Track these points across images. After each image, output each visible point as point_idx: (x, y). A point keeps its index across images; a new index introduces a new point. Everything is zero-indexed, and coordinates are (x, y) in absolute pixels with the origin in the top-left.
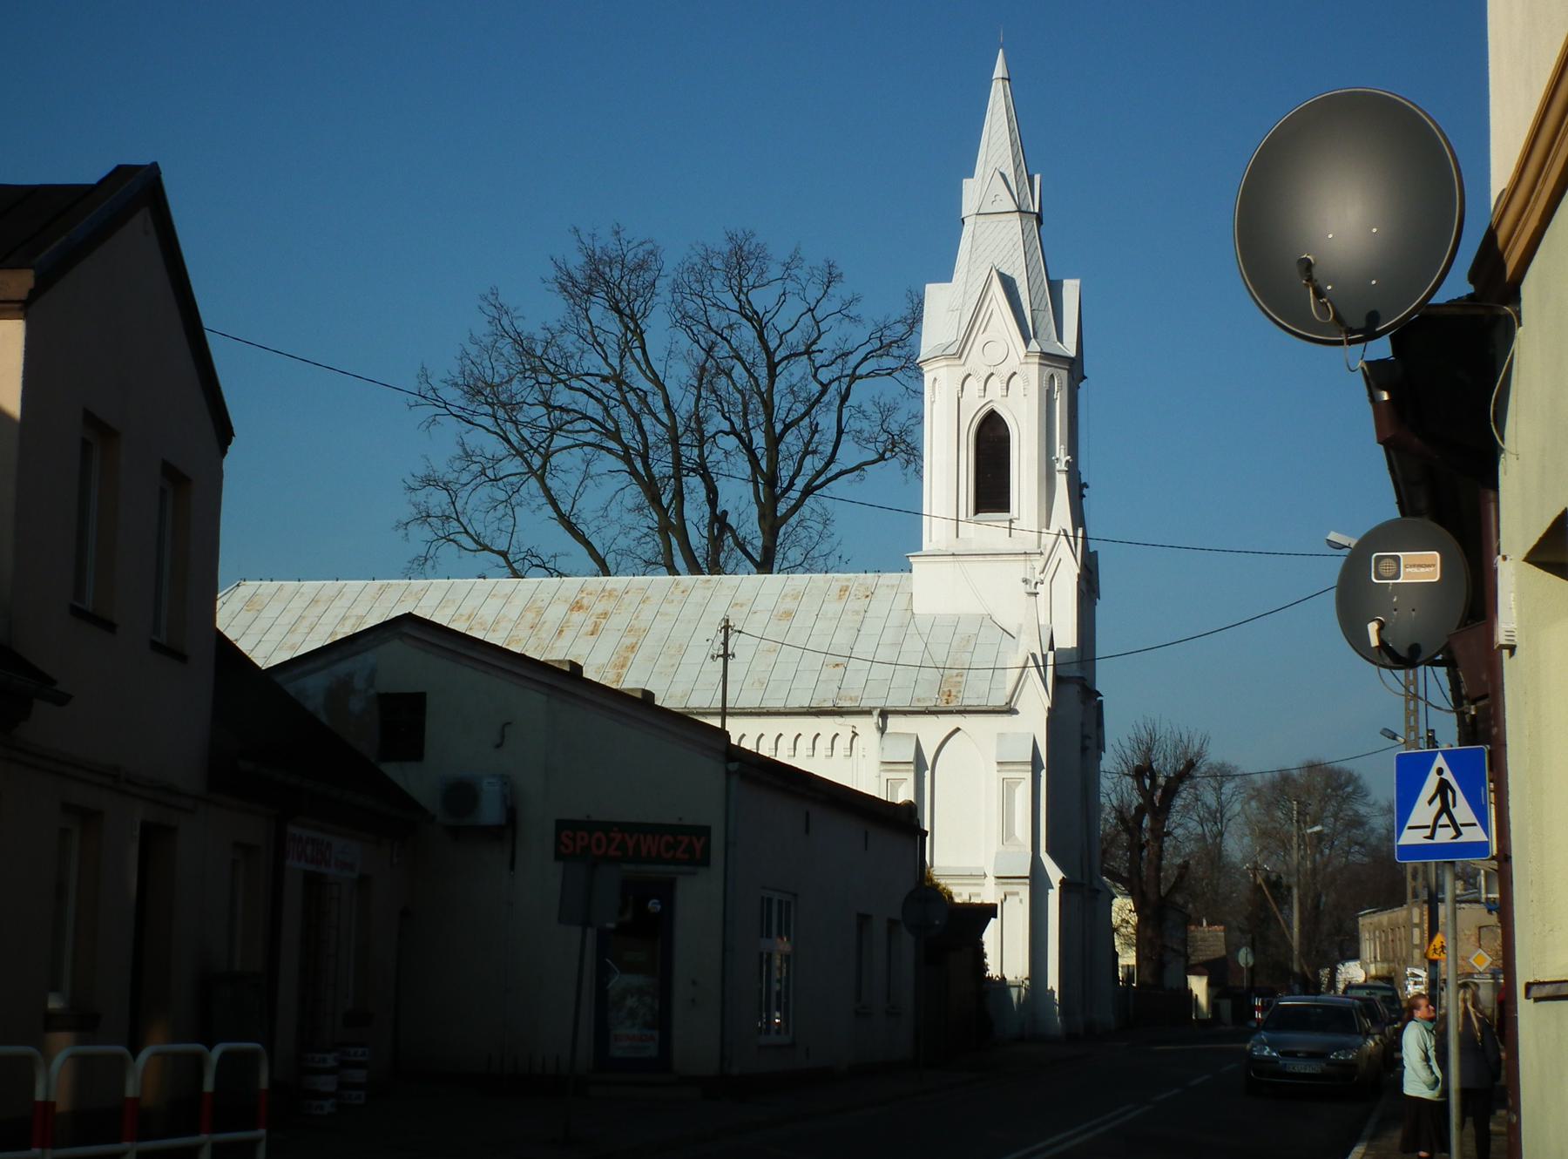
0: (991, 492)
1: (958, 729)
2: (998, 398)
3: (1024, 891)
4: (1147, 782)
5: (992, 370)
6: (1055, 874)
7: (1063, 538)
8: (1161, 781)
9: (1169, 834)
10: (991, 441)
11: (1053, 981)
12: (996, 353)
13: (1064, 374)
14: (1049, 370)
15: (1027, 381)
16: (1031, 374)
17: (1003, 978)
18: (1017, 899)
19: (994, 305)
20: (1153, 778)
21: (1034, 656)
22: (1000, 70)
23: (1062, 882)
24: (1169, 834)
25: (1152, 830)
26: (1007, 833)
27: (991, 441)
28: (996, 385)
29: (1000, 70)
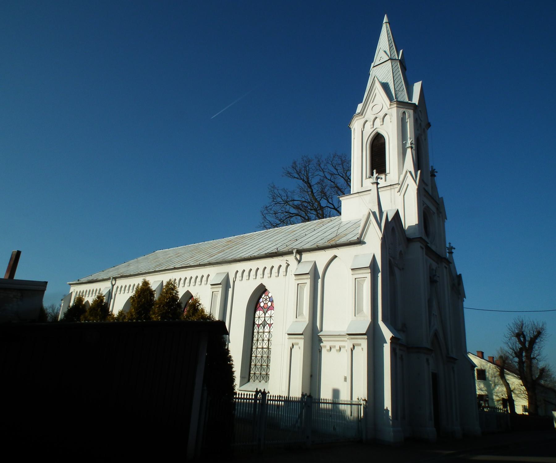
0: (378, 163)
1: (335, 257)
2: (379, 126)
3: (364, 343)
4: (522, 339)
5: (376, 115)
6: (387, 334)
7: (408, 174)
8: (528, 338)
9: (534, 358)
10: (377, 146)
11: (388, 404)
12: (377, 109)
13: (411, 112)
14: (402, 110)
15: (391, 115)
16: (394, 112)
17: (310, 399)
18: (360, 348)
19: (376, 91)
20: (524, 337)
21: (374, 213)
22: (385, 19)
23: (392, 339)
24: (534, 358)
25: (526, 356)
26: (357, 310)
27: (377, 146)
28: (378, 122)
29: (385, 19)
